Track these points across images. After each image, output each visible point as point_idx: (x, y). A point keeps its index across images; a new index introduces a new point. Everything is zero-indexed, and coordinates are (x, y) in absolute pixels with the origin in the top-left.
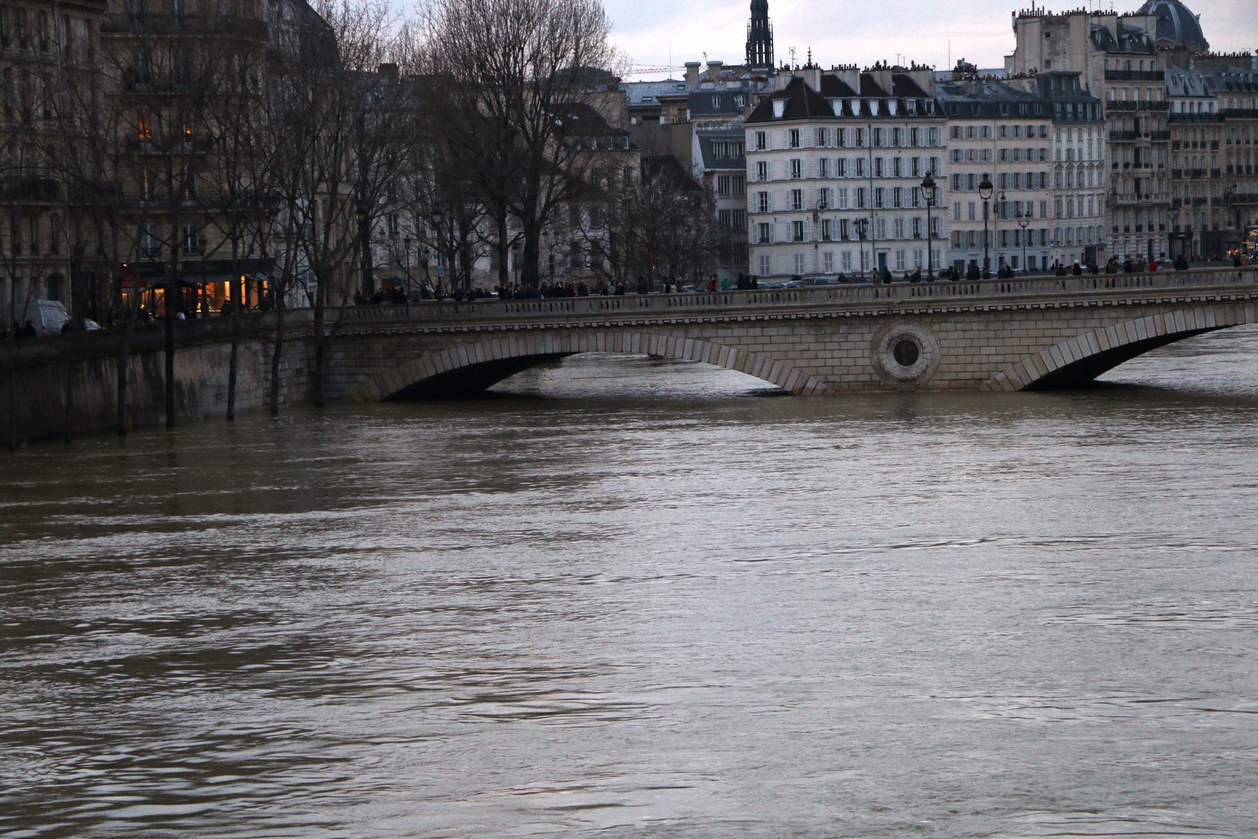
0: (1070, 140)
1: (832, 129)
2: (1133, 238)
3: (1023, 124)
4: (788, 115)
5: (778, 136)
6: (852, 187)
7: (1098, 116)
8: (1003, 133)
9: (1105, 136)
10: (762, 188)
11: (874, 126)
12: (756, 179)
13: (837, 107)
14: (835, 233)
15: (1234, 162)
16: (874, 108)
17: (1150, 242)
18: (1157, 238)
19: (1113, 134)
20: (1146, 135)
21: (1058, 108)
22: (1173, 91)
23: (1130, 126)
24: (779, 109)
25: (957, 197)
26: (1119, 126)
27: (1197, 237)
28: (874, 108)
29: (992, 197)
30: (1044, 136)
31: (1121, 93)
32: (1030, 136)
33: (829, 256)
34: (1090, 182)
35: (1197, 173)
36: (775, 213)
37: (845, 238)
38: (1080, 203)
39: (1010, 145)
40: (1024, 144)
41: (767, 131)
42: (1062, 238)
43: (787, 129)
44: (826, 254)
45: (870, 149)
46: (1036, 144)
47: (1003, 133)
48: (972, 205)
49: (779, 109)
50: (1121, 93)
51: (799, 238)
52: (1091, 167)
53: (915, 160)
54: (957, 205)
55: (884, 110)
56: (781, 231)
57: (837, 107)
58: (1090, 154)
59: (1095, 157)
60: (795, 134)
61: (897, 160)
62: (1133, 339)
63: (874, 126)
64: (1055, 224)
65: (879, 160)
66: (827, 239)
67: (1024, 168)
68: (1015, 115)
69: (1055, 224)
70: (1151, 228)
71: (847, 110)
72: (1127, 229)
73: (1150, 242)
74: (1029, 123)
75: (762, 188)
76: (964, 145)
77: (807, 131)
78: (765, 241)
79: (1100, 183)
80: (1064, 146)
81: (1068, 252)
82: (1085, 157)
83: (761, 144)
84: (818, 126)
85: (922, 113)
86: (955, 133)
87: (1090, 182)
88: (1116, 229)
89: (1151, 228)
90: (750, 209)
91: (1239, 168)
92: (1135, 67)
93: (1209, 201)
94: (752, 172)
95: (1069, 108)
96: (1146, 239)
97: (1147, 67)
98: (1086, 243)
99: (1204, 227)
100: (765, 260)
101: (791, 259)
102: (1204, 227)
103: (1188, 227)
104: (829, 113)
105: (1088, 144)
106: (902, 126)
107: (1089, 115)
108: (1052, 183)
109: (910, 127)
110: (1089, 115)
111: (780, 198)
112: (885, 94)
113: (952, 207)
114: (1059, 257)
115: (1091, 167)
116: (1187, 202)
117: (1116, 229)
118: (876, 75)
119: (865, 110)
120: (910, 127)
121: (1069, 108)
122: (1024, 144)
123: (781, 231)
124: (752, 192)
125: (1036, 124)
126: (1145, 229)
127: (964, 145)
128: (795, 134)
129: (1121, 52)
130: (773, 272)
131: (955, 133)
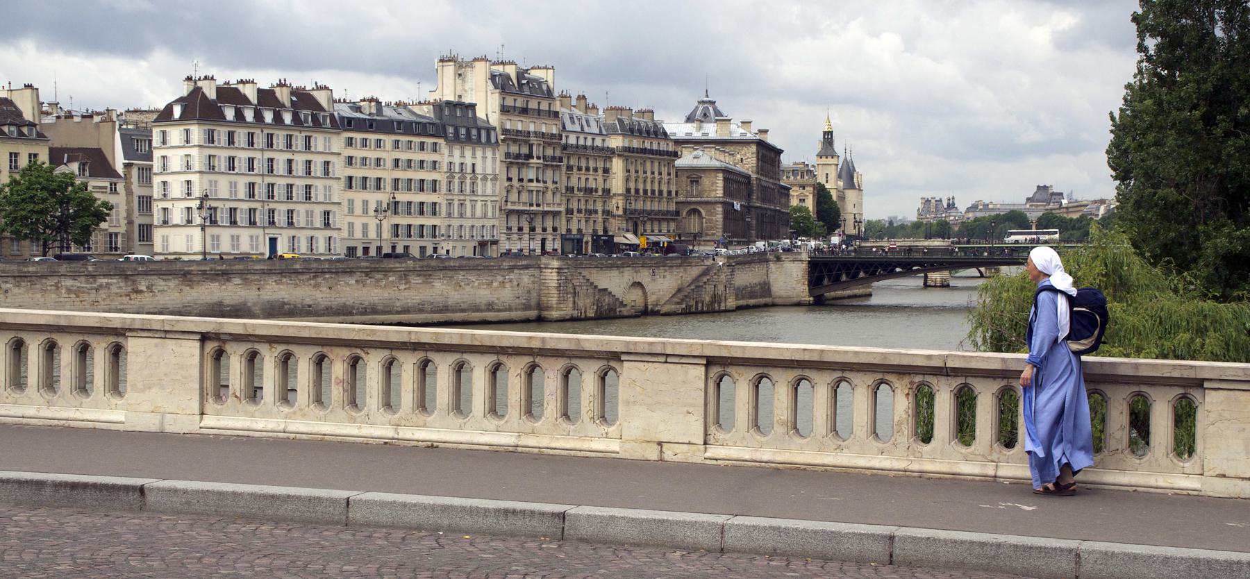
0: (462, 156)
1: (221, 133)
2: (526, 237)
3: (417, 140)
4: (184, 117)
5: (175, 134)
6: (242, 183)
7: (493, 140)
8: (396, 144)
9: (500, 155)
10: (164, 178)
11: (266, 131)
12: (161, 170)
13: (230, 113)
14: (222, 217)
15: (632, 185)
16: (268, 117)
17: (543, 241)
18: (550, 238)
19: (508, 155)
20: (538, 158)
21: (451, 130)
22: (569, 127)
23: (525, 150)
24: (177, 111)
25: (350, 194)
26: (514, 149)
27: (587, 238)
28: (268, 117)
29: (384, 197)
30: (435, 150)
31: (518, 124)
32: (422, 149)
33: (216, 238)
34: (484, 191)
35: (589, 191)
36: (173, 199)
37: (233, 223)
38: (473, 207)
39: (403, 156)
40: (417, 156)
41: (168, 129)
42: (454, 233)
43: (182, 128)
44: (213, 236)
45: (262, 150)
46: (428, 157)
47: (365, 143)
48: (365, 203)
49: (177, 111)
50: (518, 124)
51: (189, 222)
52: (485, 178)
53: (290, 162)
54: (351, 202)
55: (278, 119)
56: (177, 216)
57: (230, 113)
58: (484, 169)
59: (489, 171)
60: (187, 131)
61: (290, 162)
62: (198, 387)
63: (266, 131)
64: (447, 222)
65: (271, 160)
66: (214, 223)
67: (416, 175)
68: (424, 133)
69: (447, 222)
70: (544, 230)
71: (239, 116)
72: (520, 229)
73: (543, 241)
74: (423, 139)
75: (164, 178)
76: (358, 153)
77: (197, 132)
78: (165, 223)
79: (494, 191)
80: (457, 160)
81: (459, 245)
82: (479, 170)
83: (308, 146)
84: (207, 127)
85: (317, 124)
86: (350, 142)
87: (484, 191)
88: (509, 229)
89: (544, 230)
90: (155, 197)
91: (653, 192)
92: (647, 145)
93: (600, 212)
94: (156, 165)
95: (463, 131)
96: (539, 238)
97: (655, 147)
98: (480, 238)
99: (595, 231)
100: (165, 239)
101: (184, 238)
102: (595, 231)
103: (579, 230)
104: (221, 118)
105: (488, 162)
106: (296, 133)
107: (484, 139)
108: (443, 187)
109: (304, 134)
110: (484, 139)
111: (176, 189)
112: (283, 106)
113: (345, 203)
114: (450, 248)
115: (485, 178)
116: (579, 211)
117: (509, 229)
118: (277, 90)
119: (259, 117)
120: (304, 134)
121: (463, 131)
122: (417, 156)
123: (177, 216)
124: (157, 180)
125: (429, 141)
126: (539, 230)
127: (358, 153)
128: (187, 131)
129: (520, 93)
130: (171, 250)
131: (350, 142)
